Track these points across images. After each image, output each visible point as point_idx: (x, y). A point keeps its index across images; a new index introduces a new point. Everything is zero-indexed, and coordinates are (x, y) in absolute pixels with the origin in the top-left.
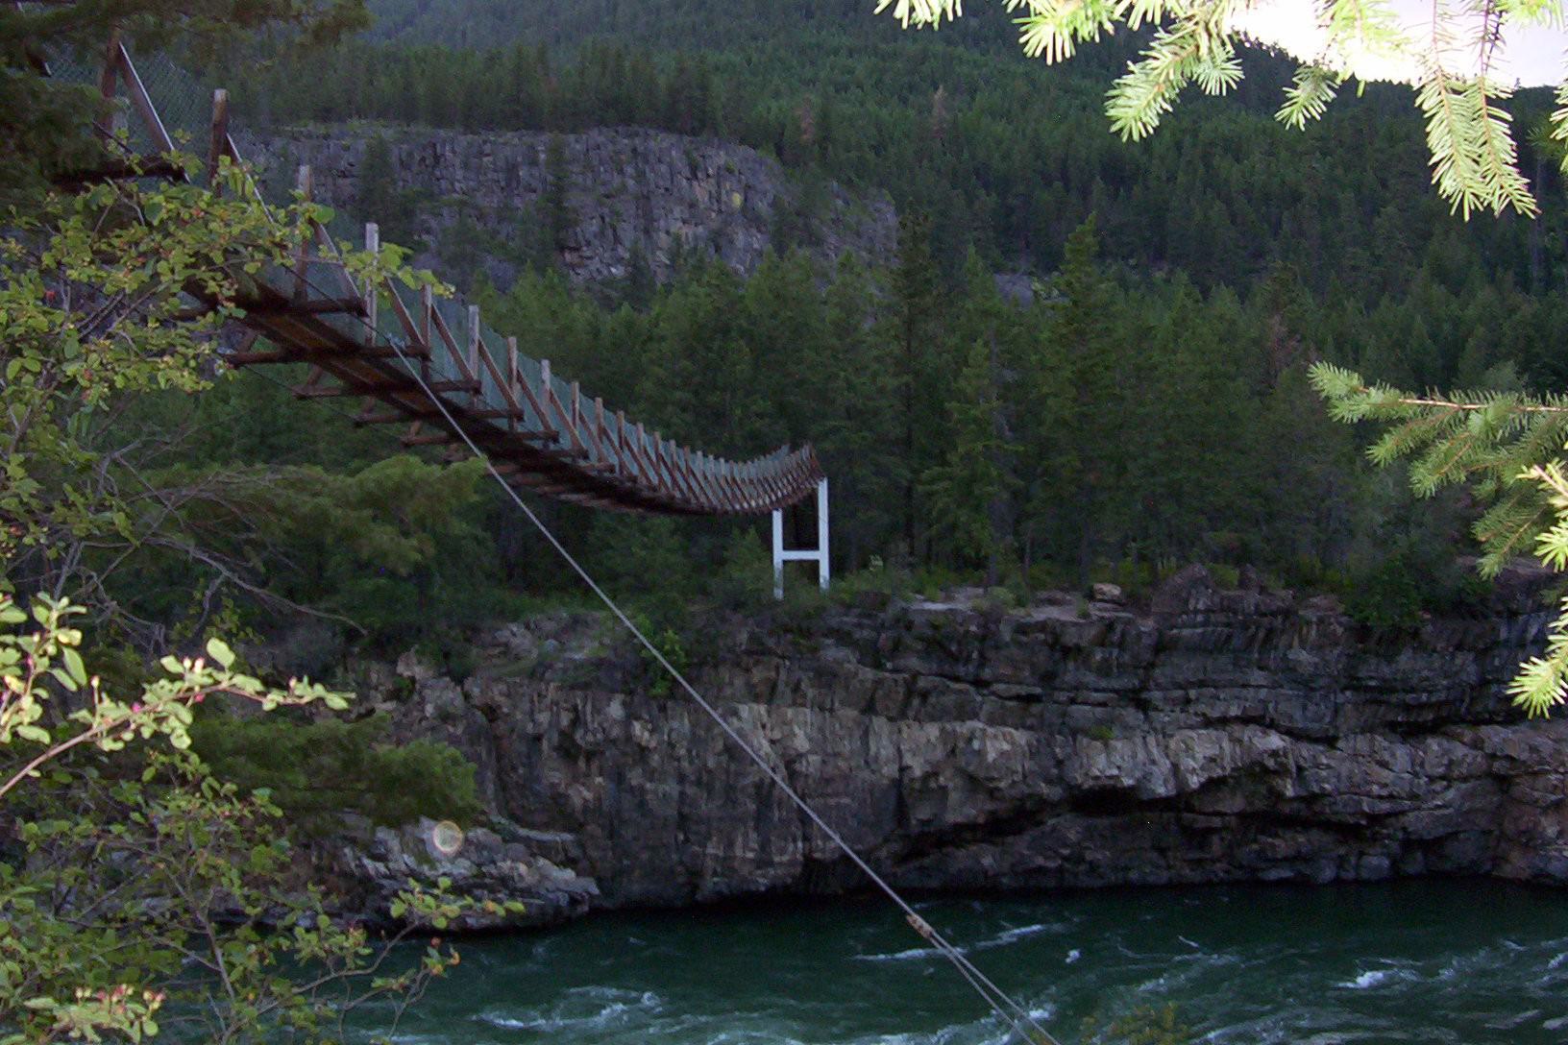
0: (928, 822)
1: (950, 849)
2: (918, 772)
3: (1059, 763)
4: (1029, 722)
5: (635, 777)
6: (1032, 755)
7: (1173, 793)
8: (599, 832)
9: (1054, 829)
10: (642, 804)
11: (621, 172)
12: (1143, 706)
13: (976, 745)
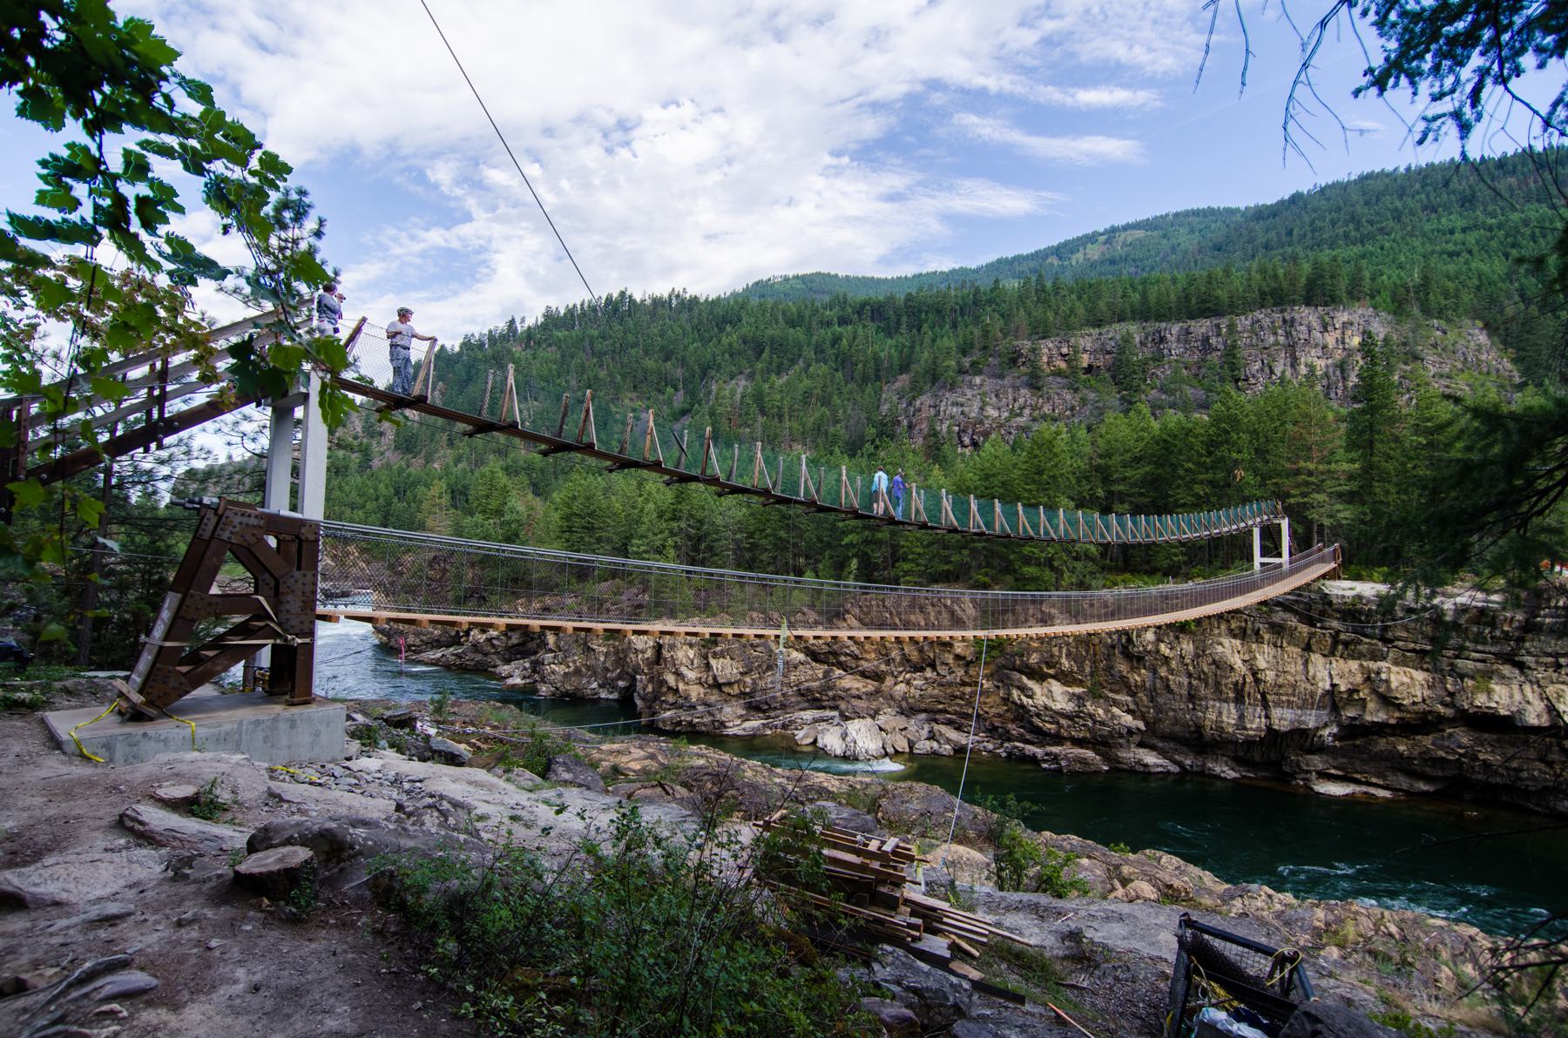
0: (1354, 719)
1: (1375, 737)
2: (1343, 688)
3: (1451, 694)
4: (1425, 666)
5: (1163, 672)
6: (1429, 687)
7: (1547, 724)
8: (1145, 698)
9: (1451, 735)
10: (1168, 686)
11: (1275, 334)
12: (1521, 666)
13: (1384, 676)
